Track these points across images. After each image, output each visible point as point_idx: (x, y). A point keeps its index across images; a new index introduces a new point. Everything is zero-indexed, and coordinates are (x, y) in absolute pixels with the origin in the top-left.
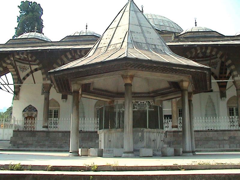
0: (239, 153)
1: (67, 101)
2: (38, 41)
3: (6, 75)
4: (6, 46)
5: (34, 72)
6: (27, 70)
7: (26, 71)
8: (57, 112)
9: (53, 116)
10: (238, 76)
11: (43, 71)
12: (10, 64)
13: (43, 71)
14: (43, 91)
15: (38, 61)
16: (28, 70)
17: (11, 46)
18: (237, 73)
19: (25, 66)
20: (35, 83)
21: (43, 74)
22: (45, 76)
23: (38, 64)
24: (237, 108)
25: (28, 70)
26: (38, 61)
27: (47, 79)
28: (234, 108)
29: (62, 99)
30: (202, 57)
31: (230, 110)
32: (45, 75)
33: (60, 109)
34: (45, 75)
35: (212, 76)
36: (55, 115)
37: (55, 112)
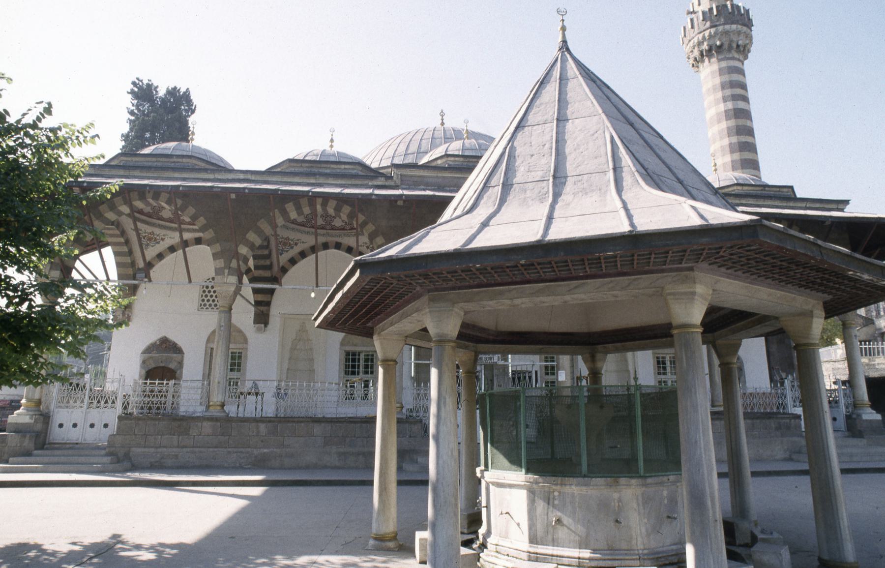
0: (881, 450)
1: (269, 326)
2: (203, 165)
3: (103, 250)
4: (107, 171)
5: (192, 245)
6: (158, 243)
7: (157, 245)
8: (240, 357)
9: (362, 369)
10: (224, 274)
11: (218, 247)
12: (113, 223)
13: (218, 247)
14: (203, 300)
15: (202, 221)
16: (161, 242)
17: (122, 172)
18: (223, 265)
19: (291, 237)
20: (190, 281)
21: (215, 256)
22: (221, 263)
23: (203, 229)
24: (674, 358)
25: (161, 242)
26: (202, 221)
27: (226, 271)
28: (668, 359)
29: (254, 323)
30: (170, 220)
31: (658, 363)
32: (222, 260)
33: (247, 349)
34: (222, 260)
35: (831, 297)
36: (366, 367)
37: (366, 360)
